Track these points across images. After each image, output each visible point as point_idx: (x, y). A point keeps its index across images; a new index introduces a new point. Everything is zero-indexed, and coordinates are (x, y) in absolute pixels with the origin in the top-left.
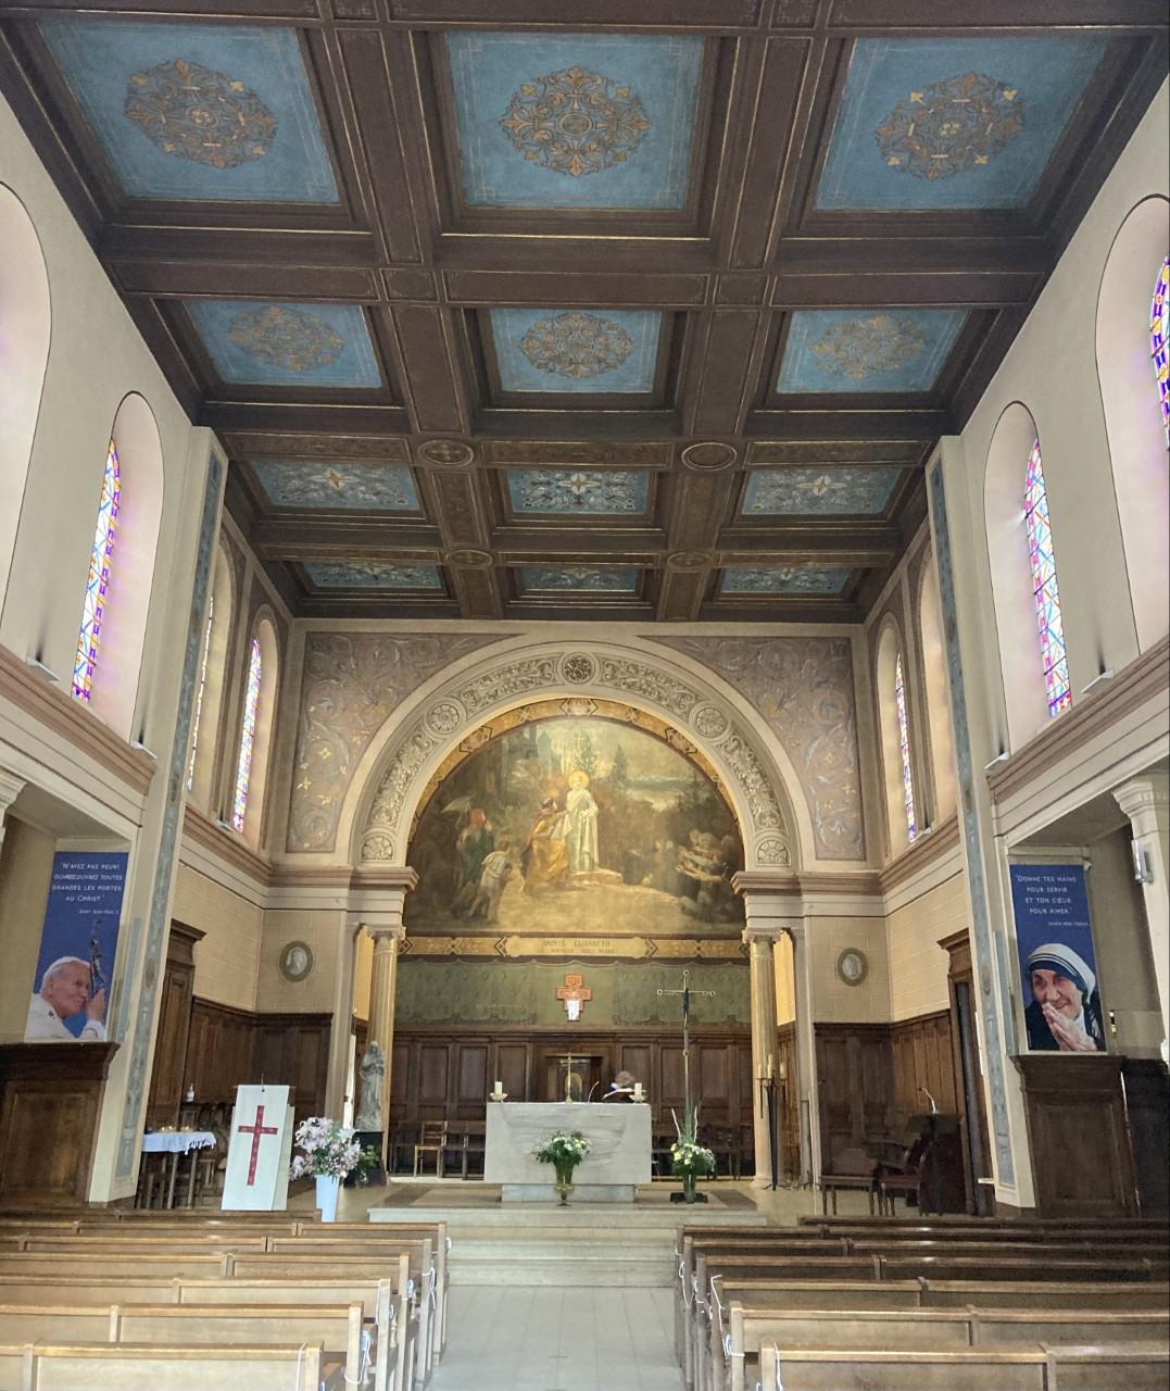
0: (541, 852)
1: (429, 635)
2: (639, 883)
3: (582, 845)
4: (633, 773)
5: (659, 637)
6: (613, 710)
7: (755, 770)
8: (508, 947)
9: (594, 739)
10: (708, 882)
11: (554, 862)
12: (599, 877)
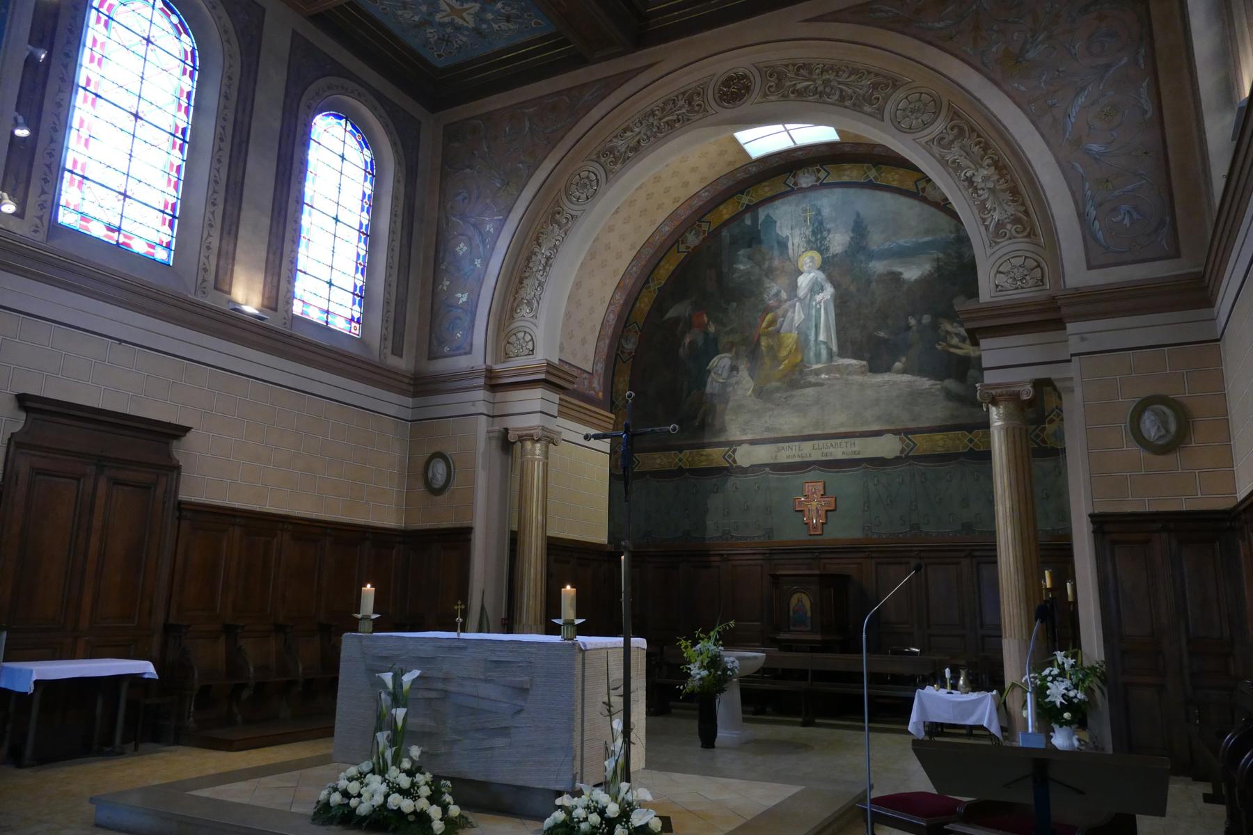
0: (770, 348)
1: (559, 93)
2: (888, 369)
3: (817, 334)
4: (876, 240)
5: (836, 12)
6: (847, 172)
7: (987, 161)
8: (738, 456)
9: (826, 212)
11: (786, 358)
12: (838, 369)
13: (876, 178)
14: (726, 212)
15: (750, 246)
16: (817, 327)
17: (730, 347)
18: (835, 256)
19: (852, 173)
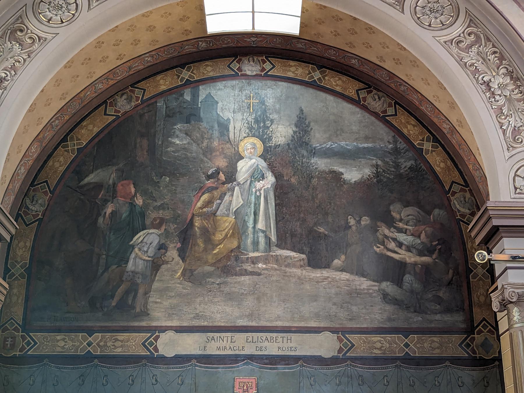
2: (327, 266)
3: (255, 221)
4: (318, 138)
8: (160, 344)
10: (415, 264)
12: (277, 259)
13: (319, 79)
14: (164, 82)
15: (188, 122)
16: (256, 214)
17: (158, 224)
18: (277, 146)
19: (296, 70)
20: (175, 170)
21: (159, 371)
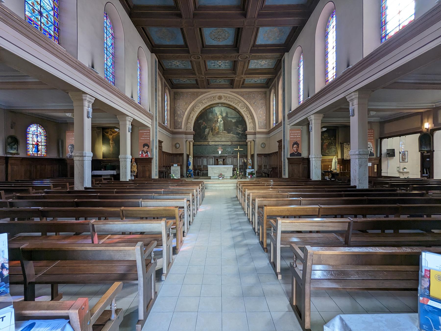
4: (229, 116)
20: (210, 120)
21: (209, 146)
